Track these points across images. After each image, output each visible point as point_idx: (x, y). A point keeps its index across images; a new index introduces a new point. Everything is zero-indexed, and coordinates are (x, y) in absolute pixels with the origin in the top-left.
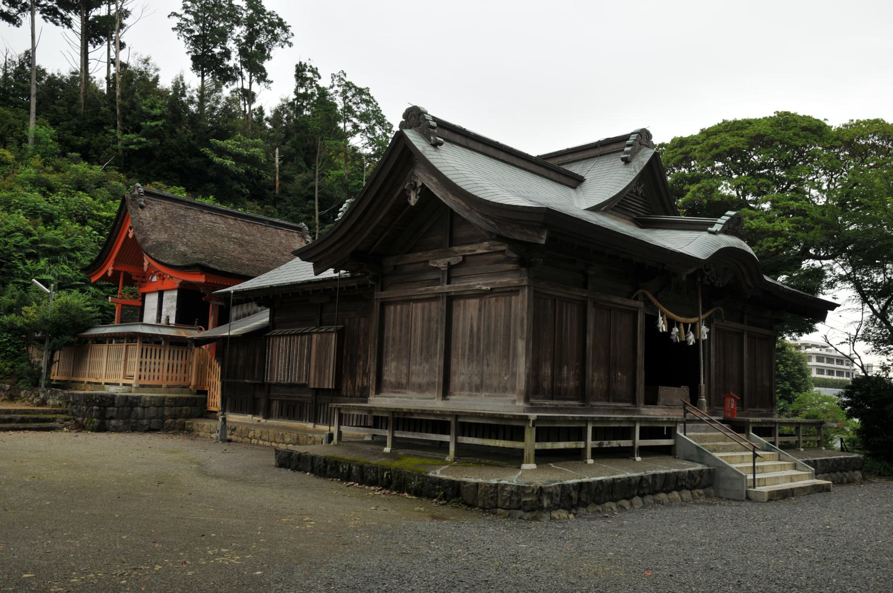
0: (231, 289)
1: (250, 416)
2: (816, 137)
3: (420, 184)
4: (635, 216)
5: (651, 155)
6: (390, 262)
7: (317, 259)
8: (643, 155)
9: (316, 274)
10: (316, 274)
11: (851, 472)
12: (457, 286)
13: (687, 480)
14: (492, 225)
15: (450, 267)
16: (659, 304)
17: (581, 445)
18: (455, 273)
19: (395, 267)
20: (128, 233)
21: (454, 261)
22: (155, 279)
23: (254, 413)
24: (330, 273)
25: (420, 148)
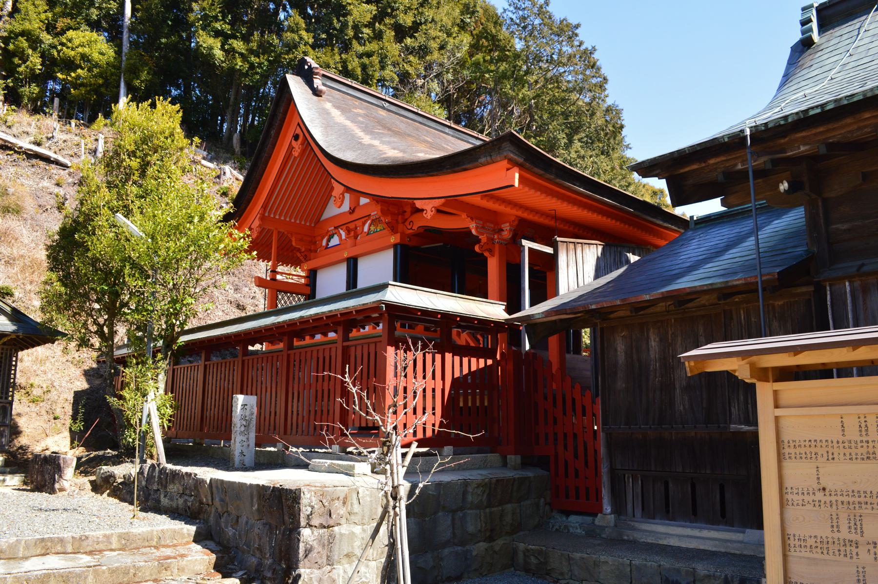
20: (291, 148)
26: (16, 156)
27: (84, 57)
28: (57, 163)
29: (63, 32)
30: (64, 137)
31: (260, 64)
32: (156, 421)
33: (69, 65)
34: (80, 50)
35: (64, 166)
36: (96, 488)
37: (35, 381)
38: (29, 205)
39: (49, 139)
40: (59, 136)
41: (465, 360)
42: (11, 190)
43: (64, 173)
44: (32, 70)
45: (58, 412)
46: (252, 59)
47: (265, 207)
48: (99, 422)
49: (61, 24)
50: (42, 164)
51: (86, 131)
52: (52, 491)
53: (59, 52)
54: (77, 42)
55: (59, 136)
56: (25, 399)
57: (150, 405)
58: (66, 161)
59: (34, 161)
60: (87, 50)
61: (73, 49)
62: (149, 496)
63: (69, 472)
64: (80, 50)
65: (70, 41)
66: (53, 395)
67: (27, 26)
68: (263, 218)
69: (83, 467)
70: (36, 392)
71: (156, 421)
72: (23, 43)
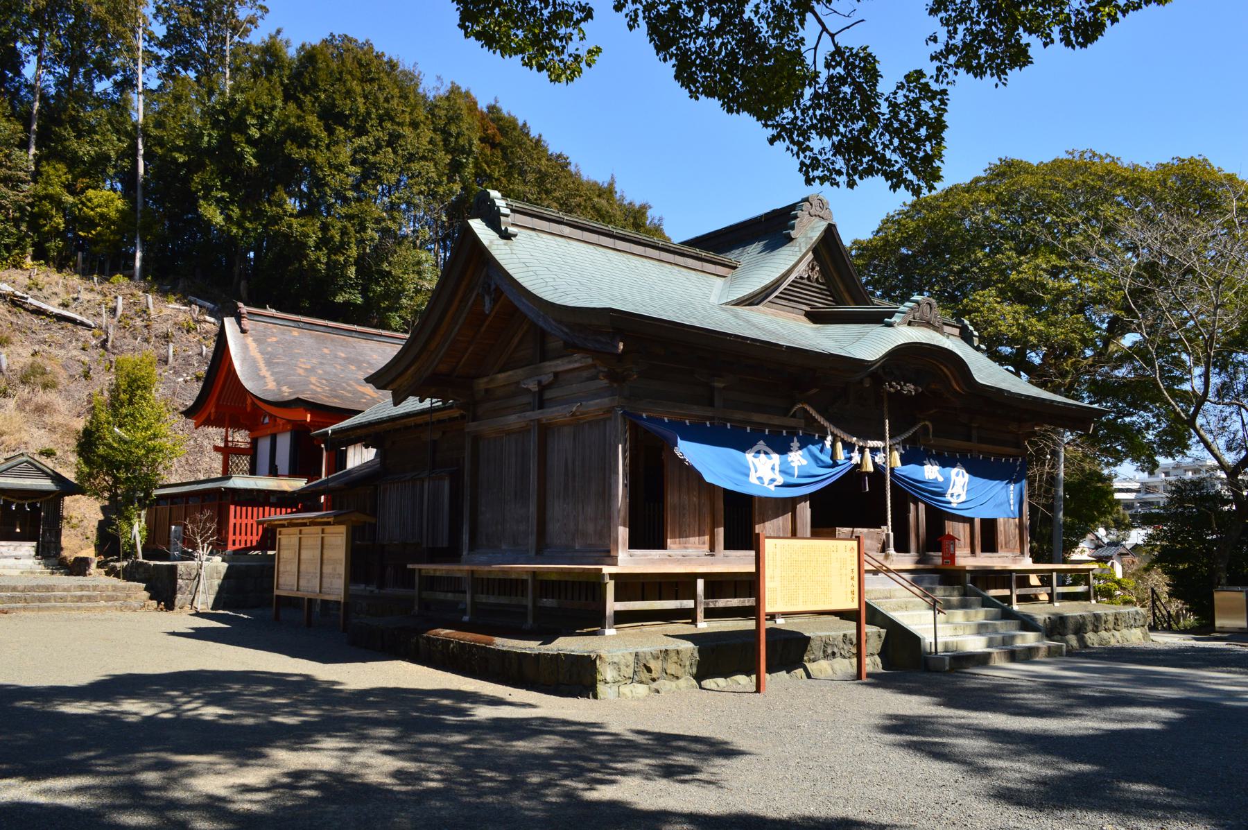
0: (329, 430)
1: (362, 586)
2: (934, 204)
3: (493, 287)
4: (808, 309)
5: (823, 228)
6: (482, 383)
7: (395, 386)
8: (813, 229)
9: (396, 404)
10: (396, 404)
11: (1125, 631)
12: (555, 413)
13: (841, 645)
14: (566, 334)
15: (543, 388)
16: (826, 424)
17: (689, 604)
18: (548, 394)
19: (487, 391)
21: (546, 379)
22: (267, 420)
23: (367, 583)
24: (412, 404)
25: (486, 242)
26: (48, 320)
27: (102, 216)
28: (82, 324)
29: (83, 191)
30: (89, 296)
31: (255, 229)
32: (138, 539)
33: (89, 223)
34: (98, 210)
35: (88, 327)
36: (107, 574)
37: (74, 514)
38: (62, 377)
39: (75, 300)
40: (85, 296)
41: (255, 509)
42: (48, 369)
43: (88, 334)
44: (57, 228)
45: (89, 534)
46: (247, 224)
47: (219, 399)
48: (108, 542)
49: (79, 185)
50: (70, 325)
51: (107, 285)
52: (85, 575)
53: (80, 210)
54: (95, 201)
55: (85, 296)
56: (67, 526)
57: (137, 530)
58: (89, 322)
59: (64, 324)
60: (105, 210)
61: (92, 209)
62: (129, 575)
63: (94, 566)
64: (98, 210)
65: (90, 200)
66: (85, 523)
67: (50, 190)
68: (217, 407)
69: (100, 565)
70: (74, 521)
71: (138, 539)
72: (47, 205)
